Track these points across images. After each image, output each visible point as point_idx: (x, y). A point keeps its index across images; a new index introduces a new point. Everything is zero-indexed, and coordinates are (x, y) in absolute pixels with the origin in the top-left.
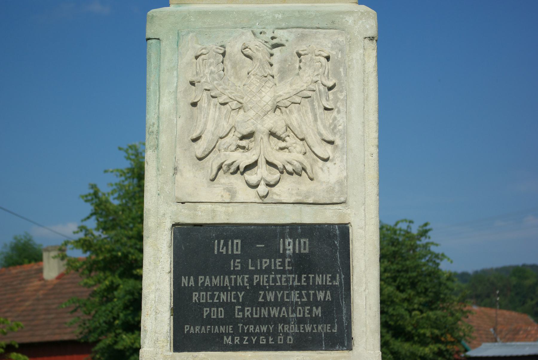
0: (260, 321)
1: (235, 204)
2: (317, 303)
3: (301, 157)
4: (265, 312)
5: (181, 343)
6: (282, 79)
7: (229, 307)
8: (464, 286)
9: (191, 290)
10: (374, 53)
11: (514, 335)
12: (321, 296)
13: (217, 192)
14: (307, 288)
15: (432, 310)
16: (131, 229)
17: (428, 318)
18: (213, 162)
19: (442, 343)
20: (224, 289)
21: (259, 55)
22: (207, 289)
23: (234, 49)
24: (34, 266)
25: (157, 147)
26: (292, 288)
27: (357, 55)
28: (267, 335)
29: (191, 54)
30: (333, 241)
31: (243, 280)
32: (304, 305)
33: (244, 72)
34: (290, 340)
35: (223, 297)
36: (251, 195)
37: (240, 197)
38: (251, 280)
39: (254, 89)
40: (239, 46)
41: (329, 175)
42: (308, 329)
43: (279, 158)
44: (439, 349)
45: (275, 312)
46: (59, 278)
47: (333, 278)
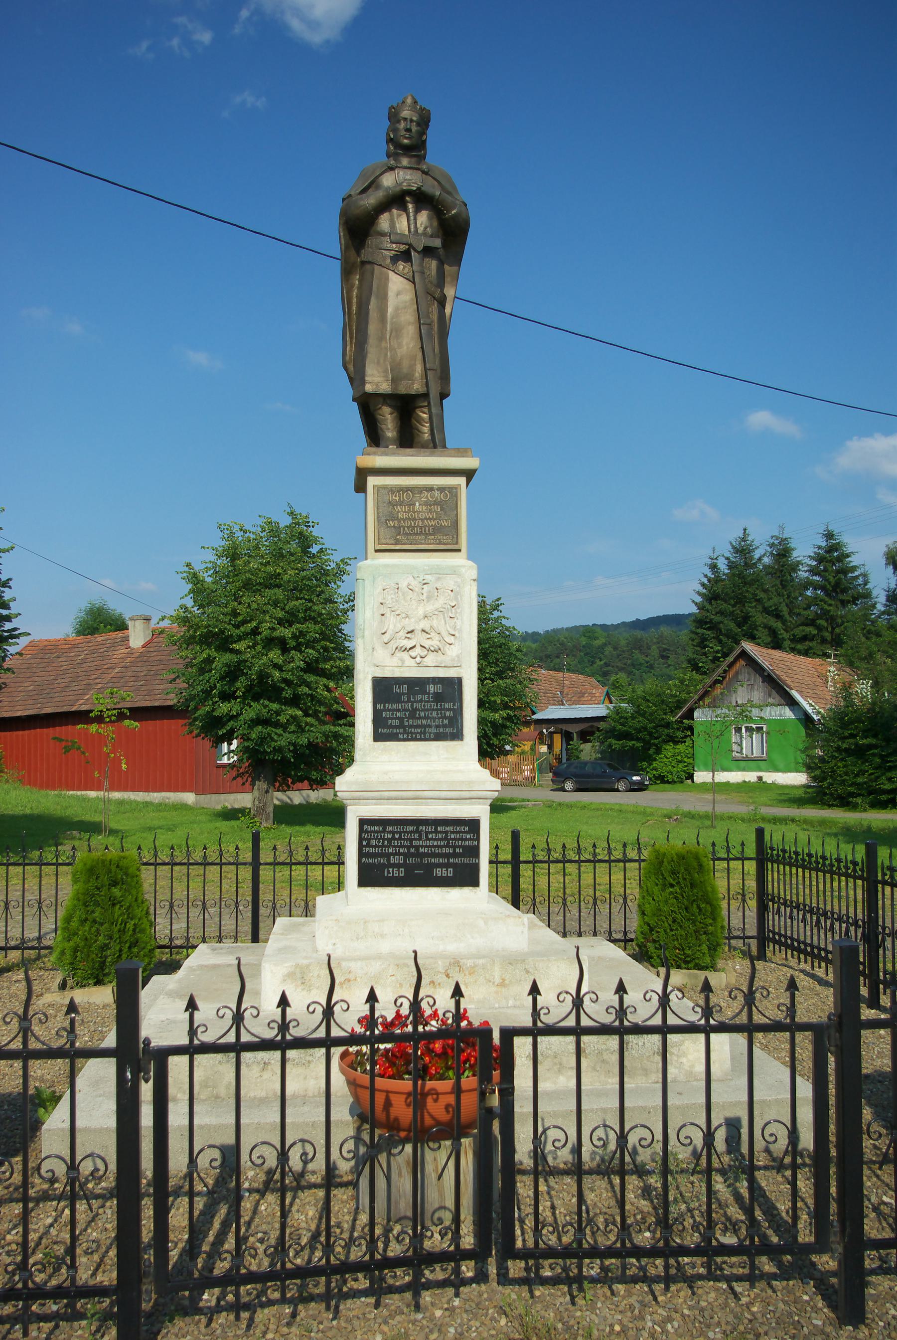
0: (417, 727)
2: (445, 717)
3: (438, 643)
4: (419, 722)
6: (428, 601)
7: (401, 719)
8: (534, 646)
9: (381, 711)
10: (476, 588)
11: (579, 699)
12: (448, 714)
13: (395, 661)
14: (441, 710)
15: (502, 678)
16: (226, 607)
17: (499, 686)
18: (393, 645)
19: (511, 708)
20: (398, 710)
21: (417, 589)
22: (390, 710)
23: (403, 585)
24: (120, 634)
25: (363, 636)
26: (433, 710)
27: (467, 589)
28: (420, 733)
29: (380, 588)
30: (453, 686)
31: (408, 706)
32: (439, 718)
33: (408, 598)
34: (432, 736)
35: (398, 714)
36: (412, 662)
37: (407, 663)
38: (412, 706)
39: (414, 607)
40: (405, 584)
41: (452, 652)
42: (441, 730)
43: (427, 644)
44: (508, 714)
45: (424, 722)
46: (144, 646)
47: (454, 705)
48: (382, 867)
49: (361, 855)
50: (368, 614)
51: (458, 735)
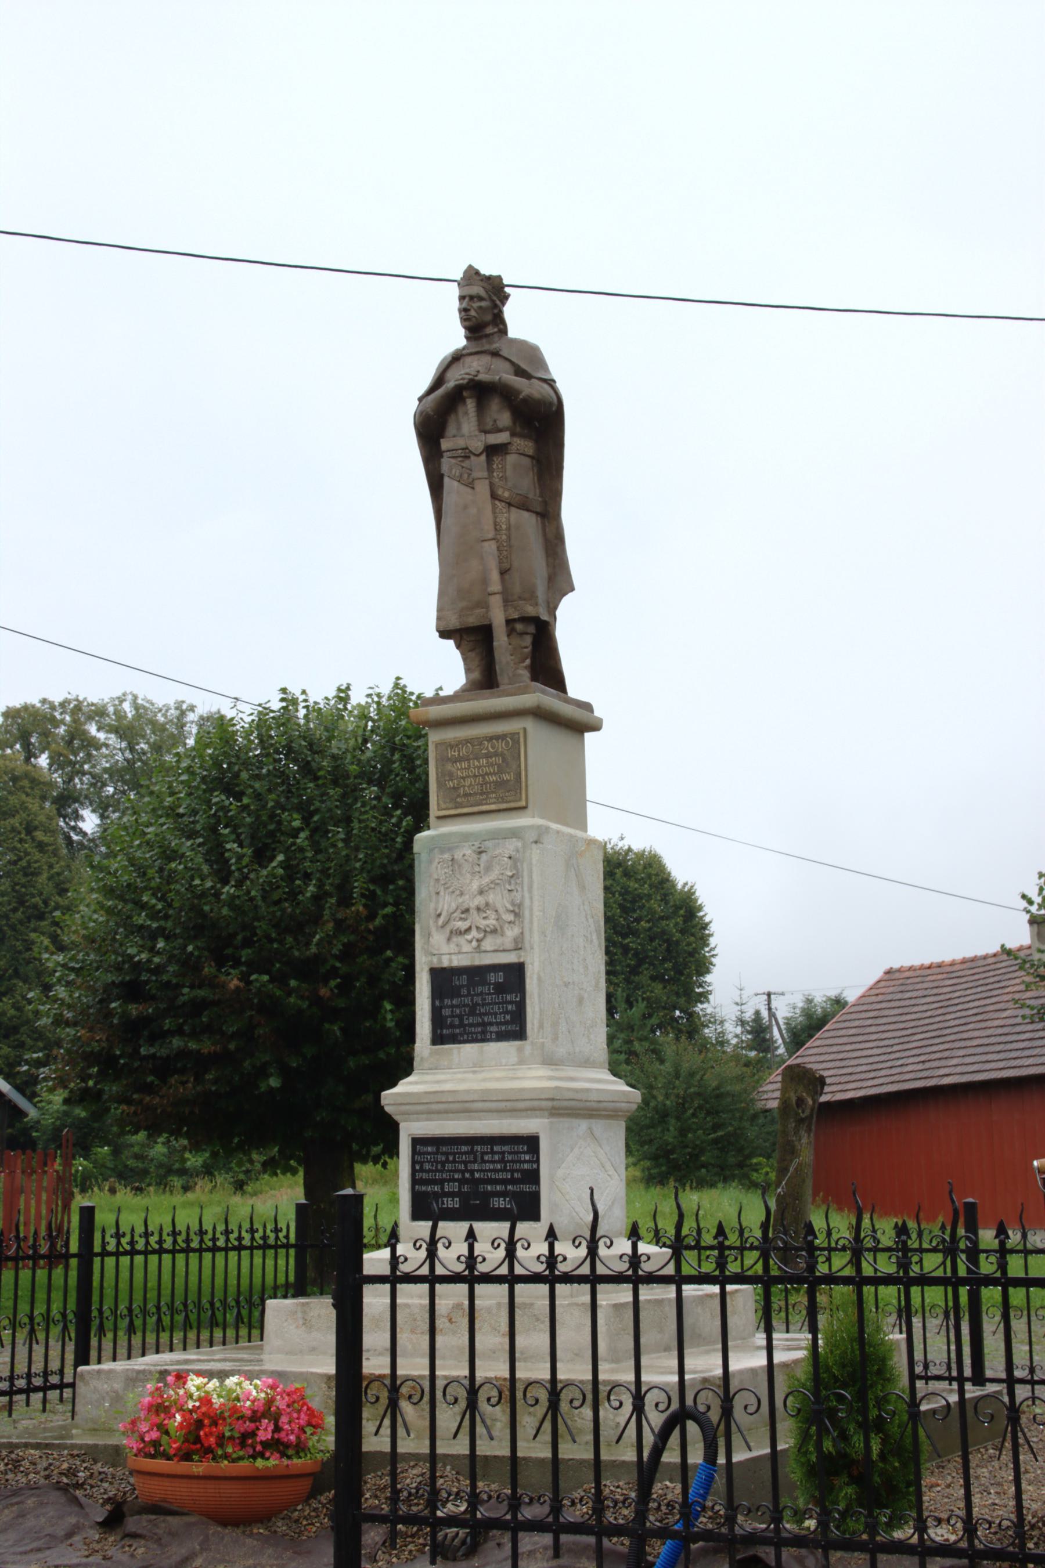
0: (478, 1025)
7: (461, 1017)
31: (467, 1001)
48: (436, 1196)
49: (415, 1181)
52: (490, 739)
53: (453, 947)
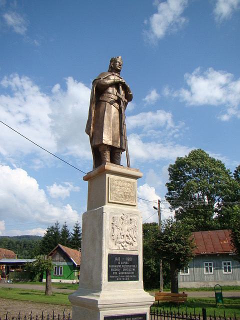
0: (123, 275)
1: (117, 250)
5: (110, 280)
7: (118, 272)
11: (9, 257)
30: (136, 257)
31: (120, 266)
43: (128, 241)
50: (108, 227)
51: (137, 279)
52: (127, 182)
53: (117, 248)
